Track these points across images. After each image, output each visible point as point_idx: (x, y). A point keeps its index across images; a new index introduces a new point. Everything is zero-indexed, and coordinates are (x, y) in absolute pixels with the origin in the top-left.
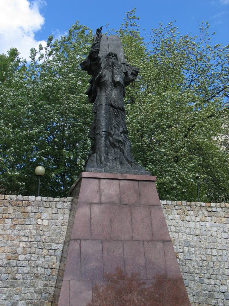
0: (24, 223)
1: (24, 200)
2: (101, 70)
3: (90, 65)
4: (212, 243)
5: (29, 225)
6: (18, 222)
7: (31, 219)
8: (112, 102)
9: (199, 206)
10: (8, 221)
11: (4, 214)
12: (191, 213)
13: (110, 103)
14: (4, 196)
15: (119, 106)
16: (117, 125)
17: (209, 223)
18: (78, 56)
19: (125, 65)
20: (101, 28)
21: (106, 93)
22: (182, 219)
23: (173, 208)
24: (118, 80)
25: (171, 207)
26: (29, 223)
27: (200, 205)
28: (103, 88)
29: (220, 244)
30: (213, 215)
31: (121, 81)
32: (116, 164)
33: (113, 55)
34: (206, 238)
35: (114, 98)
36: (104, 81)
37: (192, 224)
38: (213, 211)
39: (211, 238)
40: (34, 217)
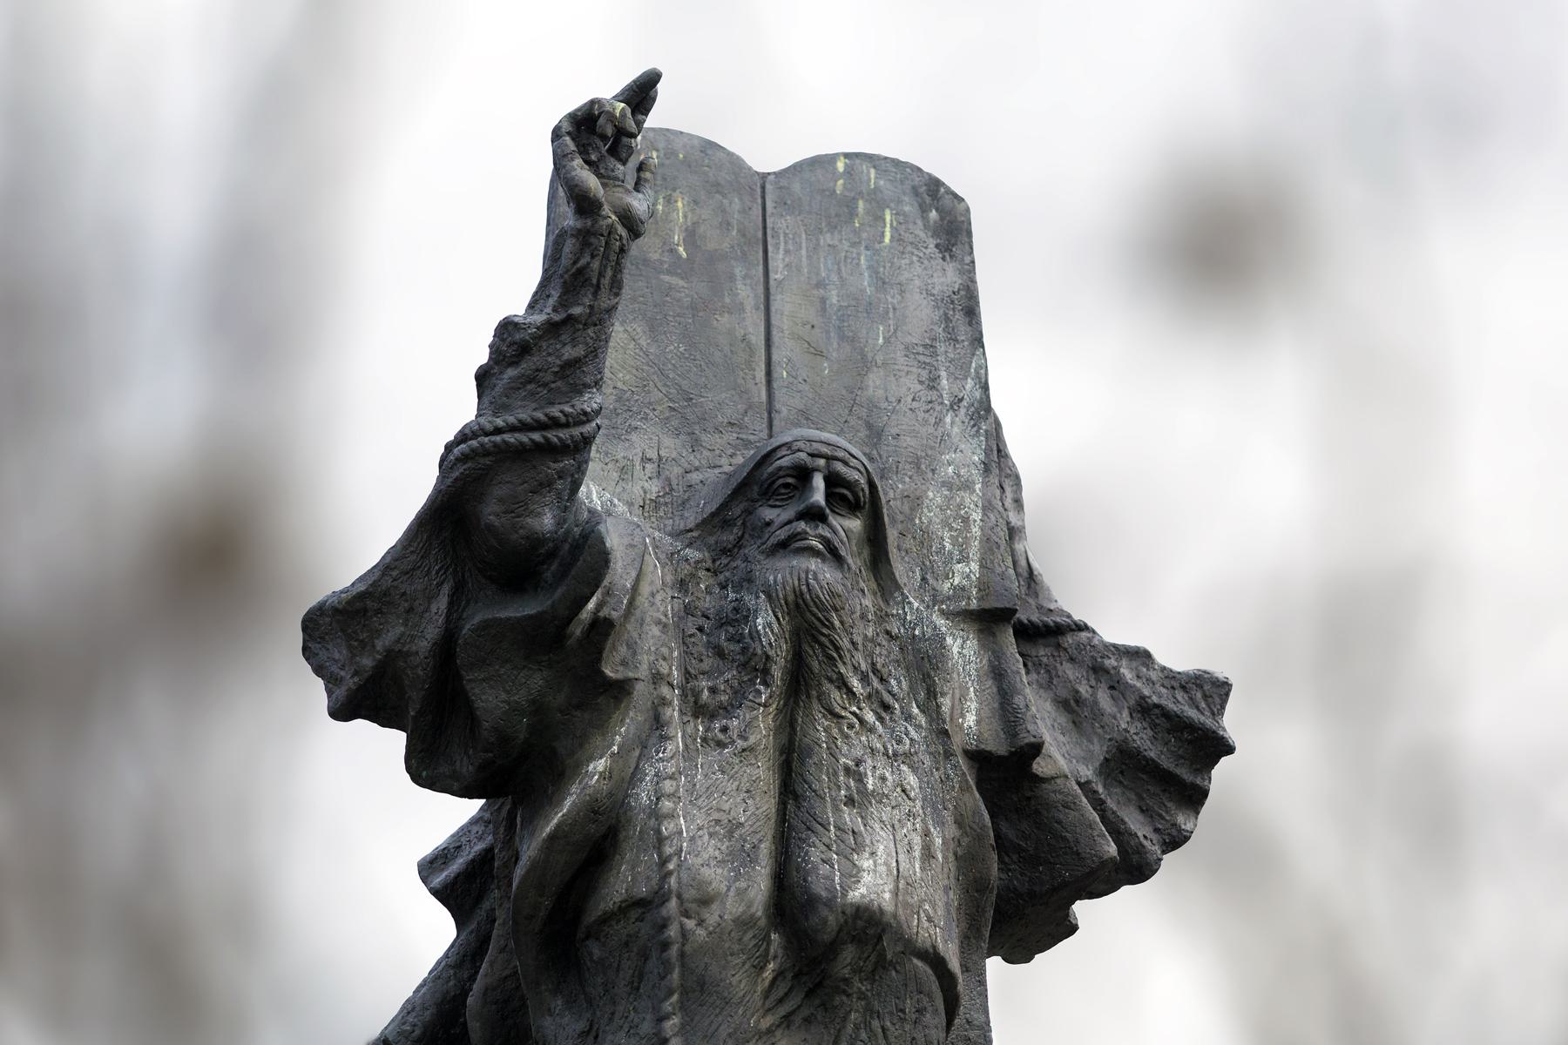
3: (447, 646)
19: (1008, 638)
20: (642, 93)
24: (857, 894)
28: (574, 173)
33: (819, 496)
36: (642, 903)
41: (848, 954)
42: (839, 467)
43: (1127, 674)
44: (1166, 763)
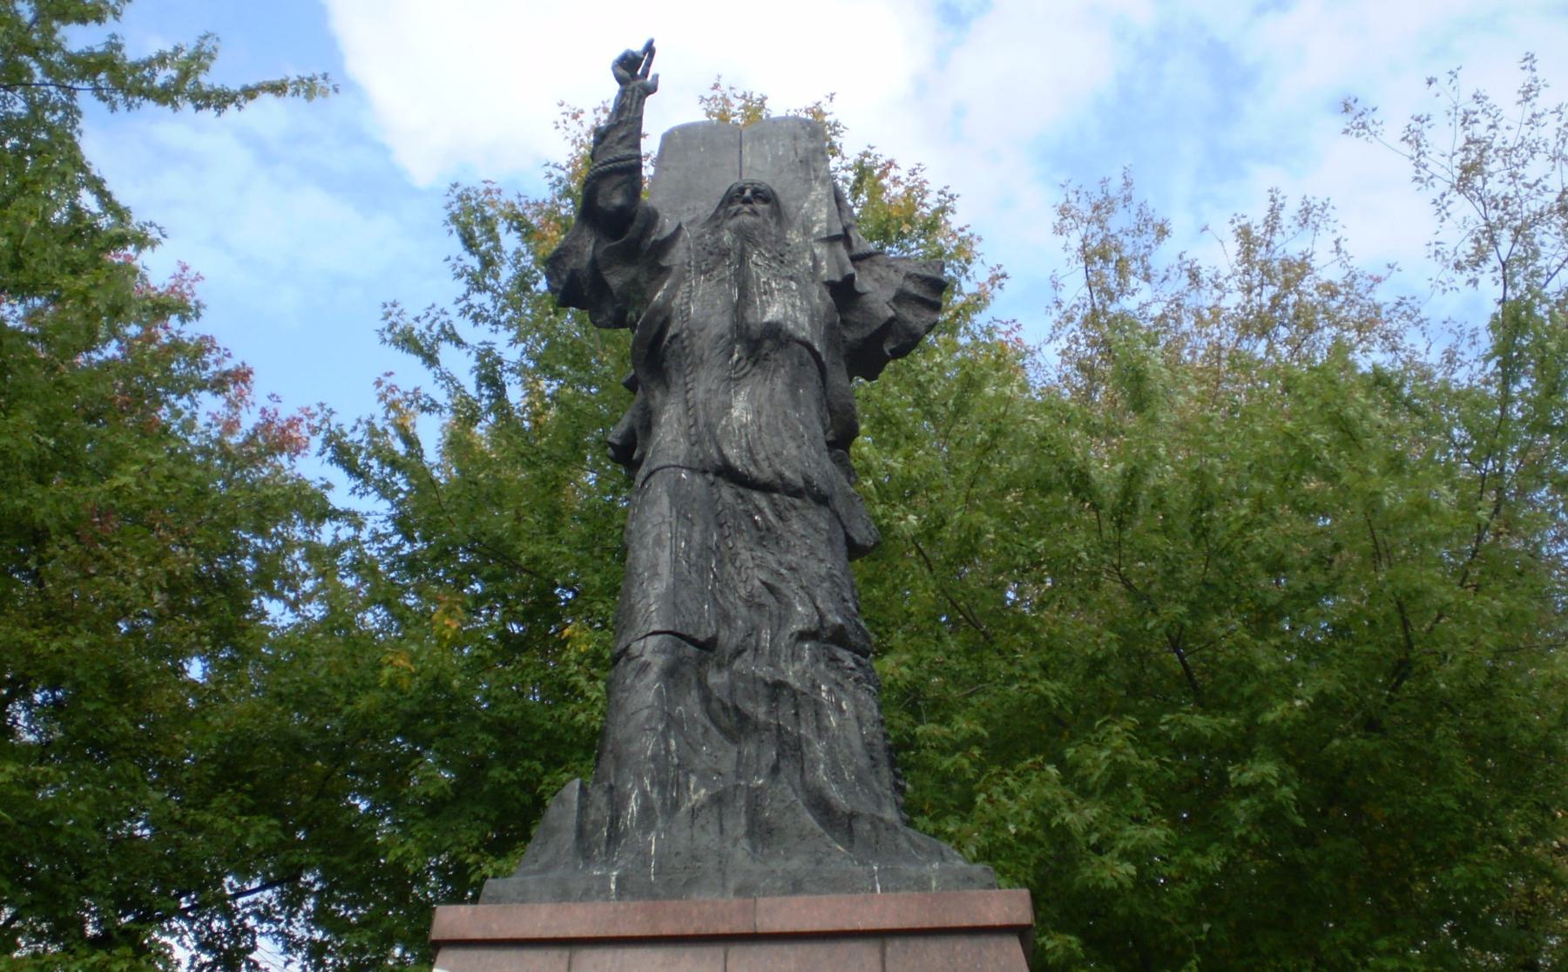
2: (663, 283)
8: (732, 454)
13: (716, 455)
15: (781, 476)
16: (771, 589)
21: (687, 401)
31: (790, 326)
32: (722, 831)
35: (744, 426)
44: (921, 294)
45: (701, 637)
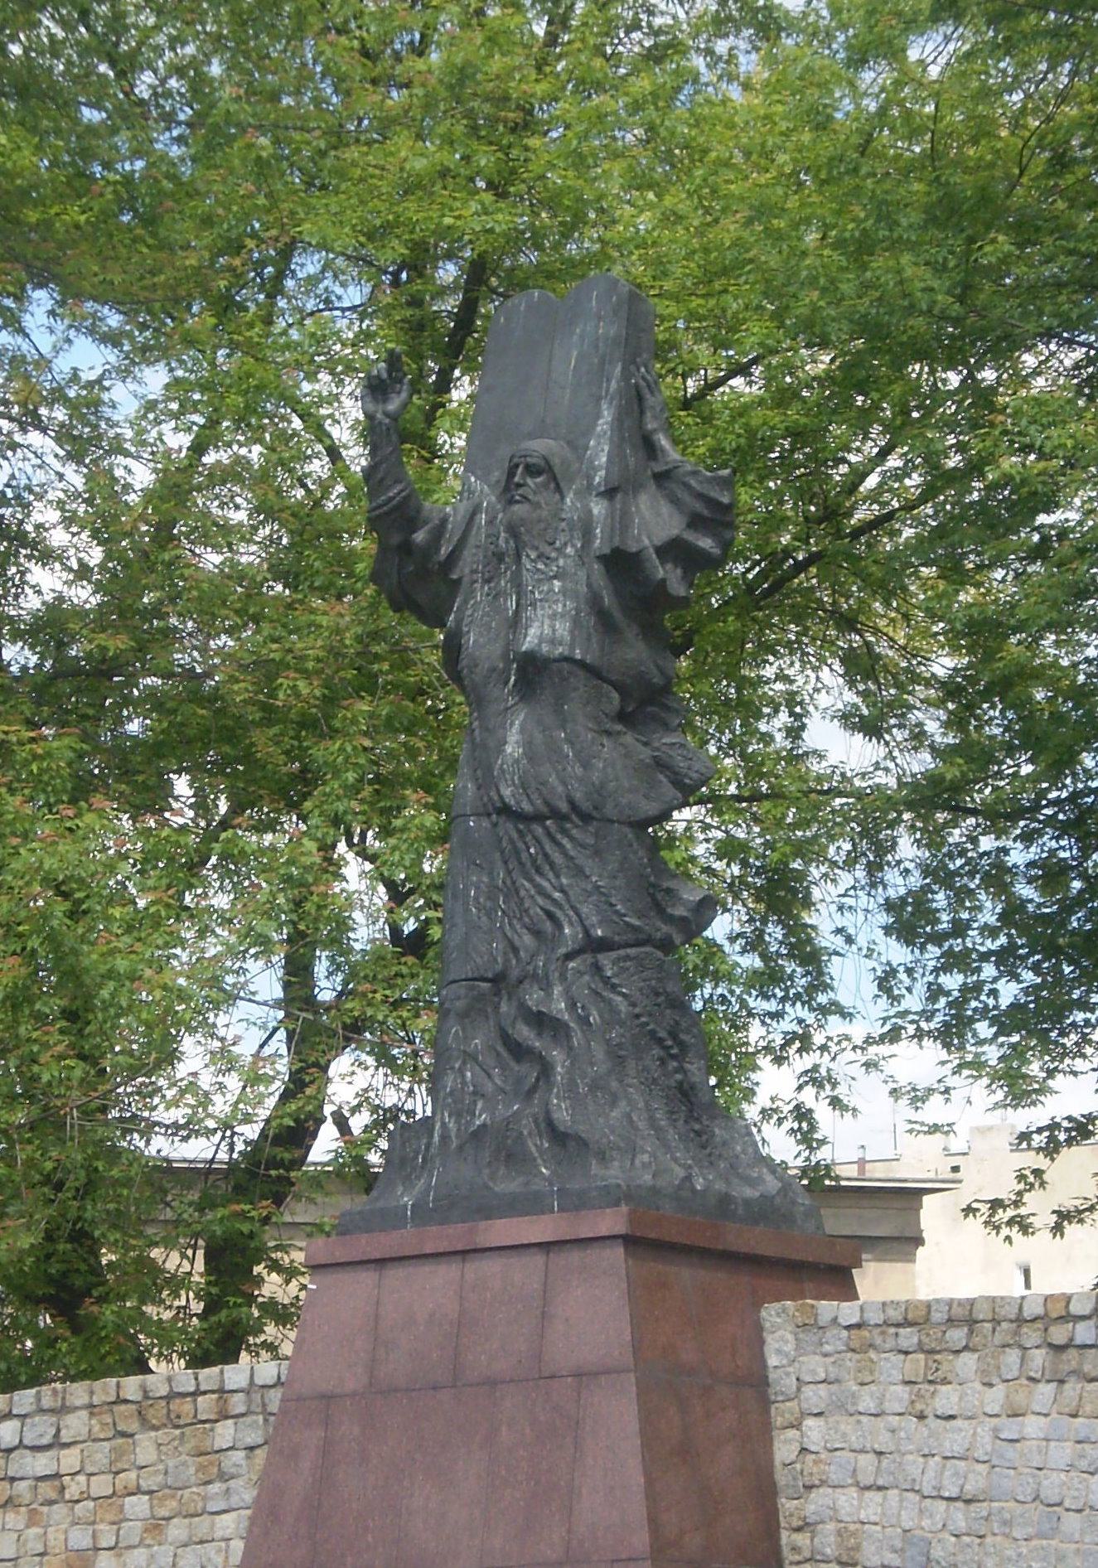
0: (200, 1505)
1: (205, 1393)
4: (1034, 1543)
5: (224, 1516)
6: (174, 1504)
7: (232, 1483)
9: (1012, 1321)
10: (138, 1506)
11: (117, 1473)
12: (968, 1363)
13: (496, 798)
14: (118, 1385)
16: (550, 916)
17: (1042, 1418)
18: (559, 68)
22: (919, 1406)
23: (888, 1346)
25: (878, 1341)
26: (222, 1506)
27: (1013, 1317)
29: (1074, 1546)
30: (1073, 1372)
34: (1007, 1516)
37: (955, 1438)
38: (1078, 1341)
39: (1036, 1512)
40: (244, 1470)
41: (530, 669)
42: (529, 459)
43: (693, 483)
45: (490, 975)
